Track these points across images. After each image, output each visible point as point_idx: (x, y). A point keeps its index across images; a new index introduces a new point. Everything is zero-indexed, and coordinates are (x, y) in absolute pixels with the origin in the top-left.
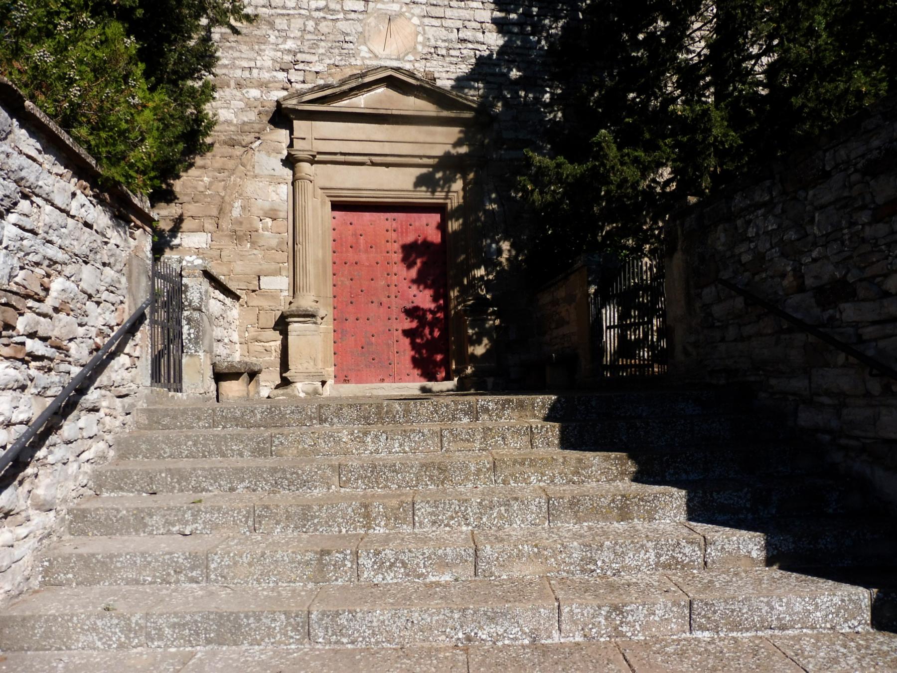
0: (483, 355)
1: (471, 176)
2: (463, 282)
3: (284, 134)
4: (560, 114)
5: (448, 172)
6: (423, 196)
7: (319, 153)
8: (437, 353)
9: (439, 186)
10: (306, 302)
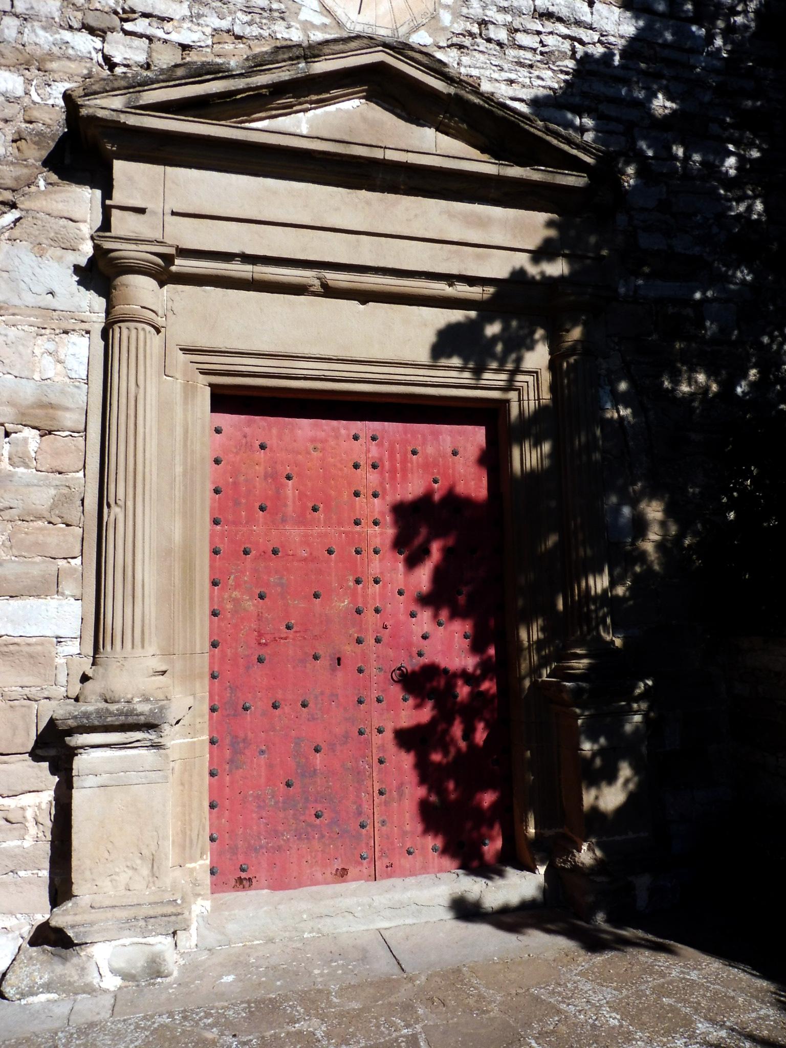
0: (621, 811)
1: (576, 333)
2: (555, 605)
3: (83, 201)
4: (759, 206)
5: (514, 323)
6: (452, 380)
7: (184, 253)
8: (484, 788)
9: (494, 356)
10: (133, 677)
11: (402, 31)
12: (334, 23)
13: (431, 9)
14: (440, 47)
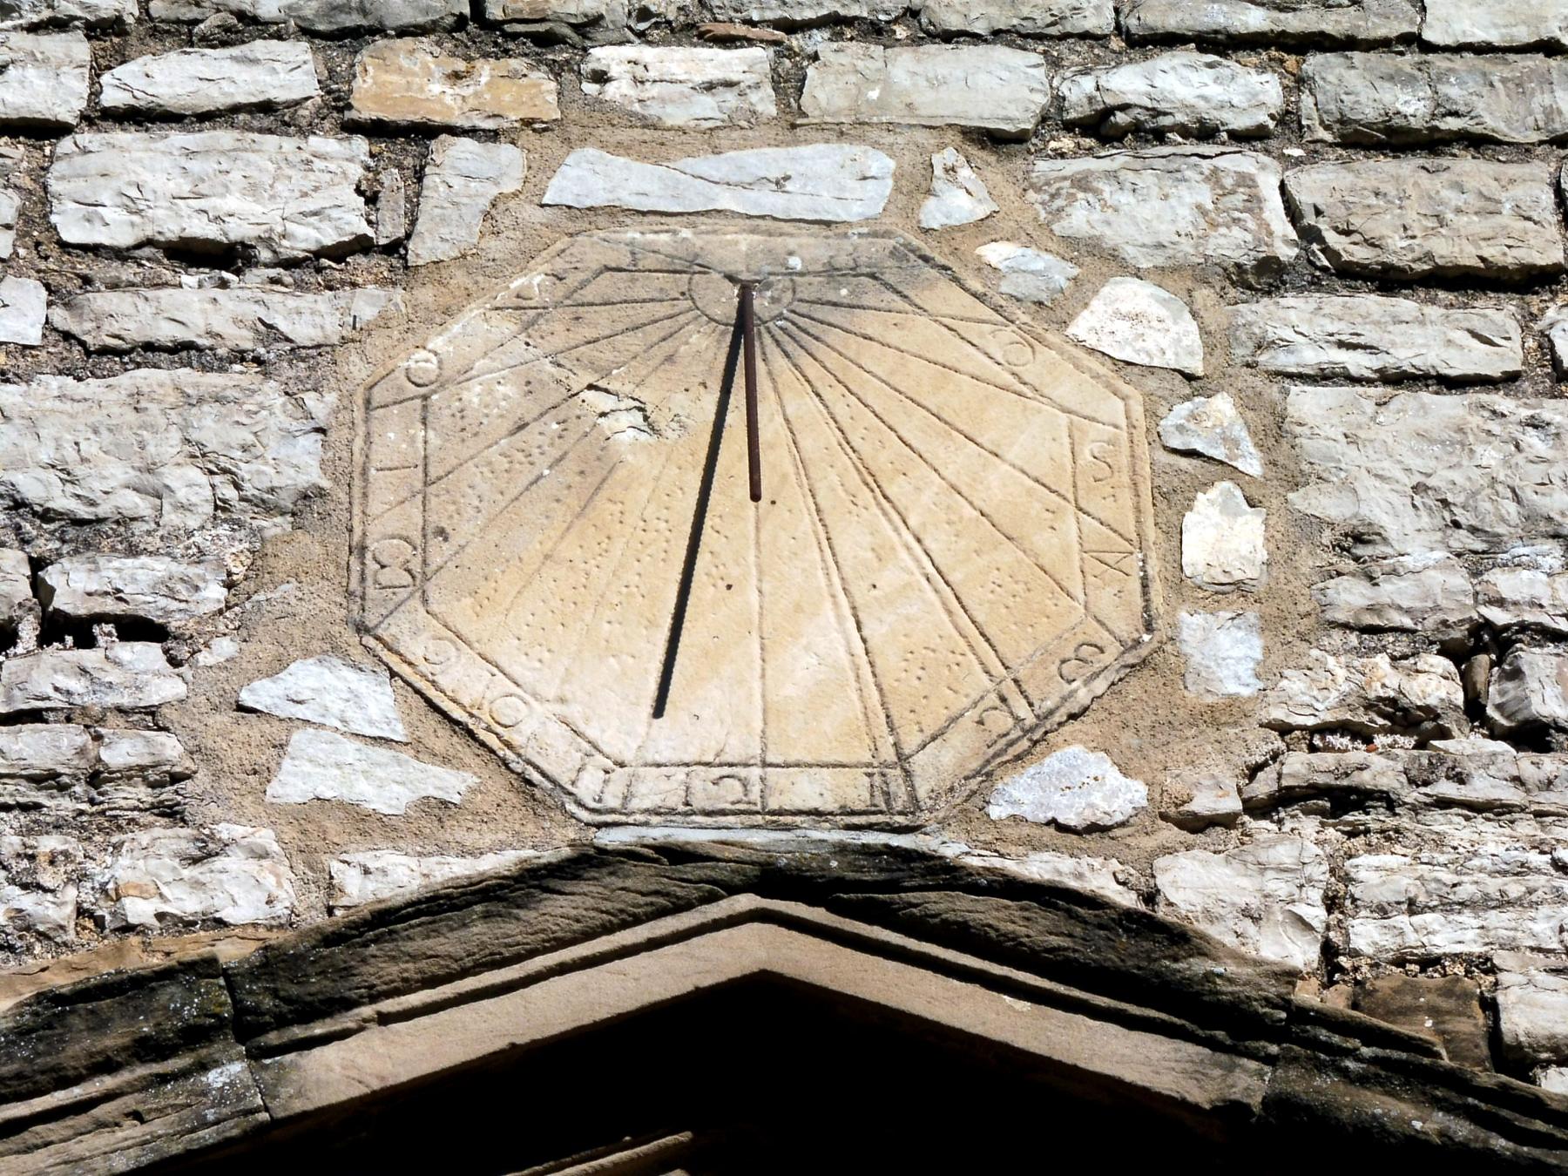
11: (937, 767)
12: (498, 785)
13: (1125, 624)
14: (1197, 824)
